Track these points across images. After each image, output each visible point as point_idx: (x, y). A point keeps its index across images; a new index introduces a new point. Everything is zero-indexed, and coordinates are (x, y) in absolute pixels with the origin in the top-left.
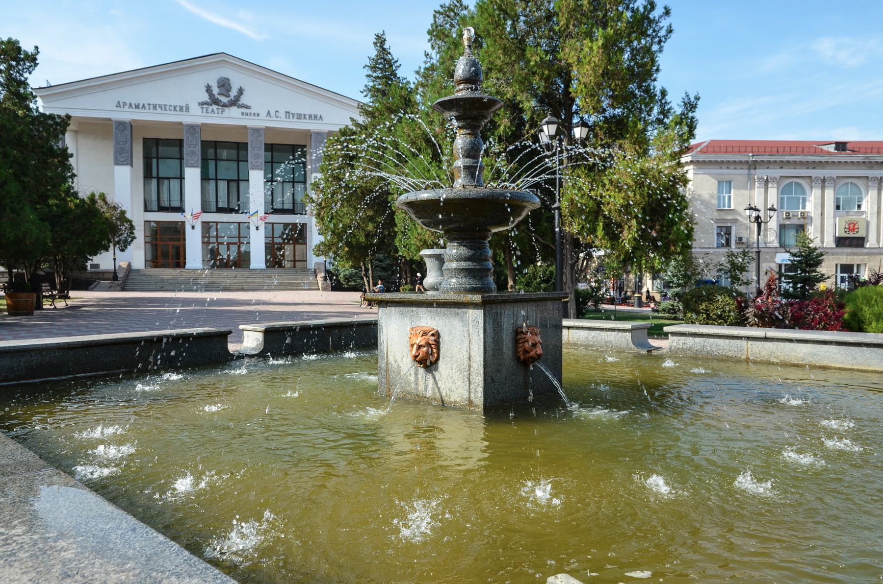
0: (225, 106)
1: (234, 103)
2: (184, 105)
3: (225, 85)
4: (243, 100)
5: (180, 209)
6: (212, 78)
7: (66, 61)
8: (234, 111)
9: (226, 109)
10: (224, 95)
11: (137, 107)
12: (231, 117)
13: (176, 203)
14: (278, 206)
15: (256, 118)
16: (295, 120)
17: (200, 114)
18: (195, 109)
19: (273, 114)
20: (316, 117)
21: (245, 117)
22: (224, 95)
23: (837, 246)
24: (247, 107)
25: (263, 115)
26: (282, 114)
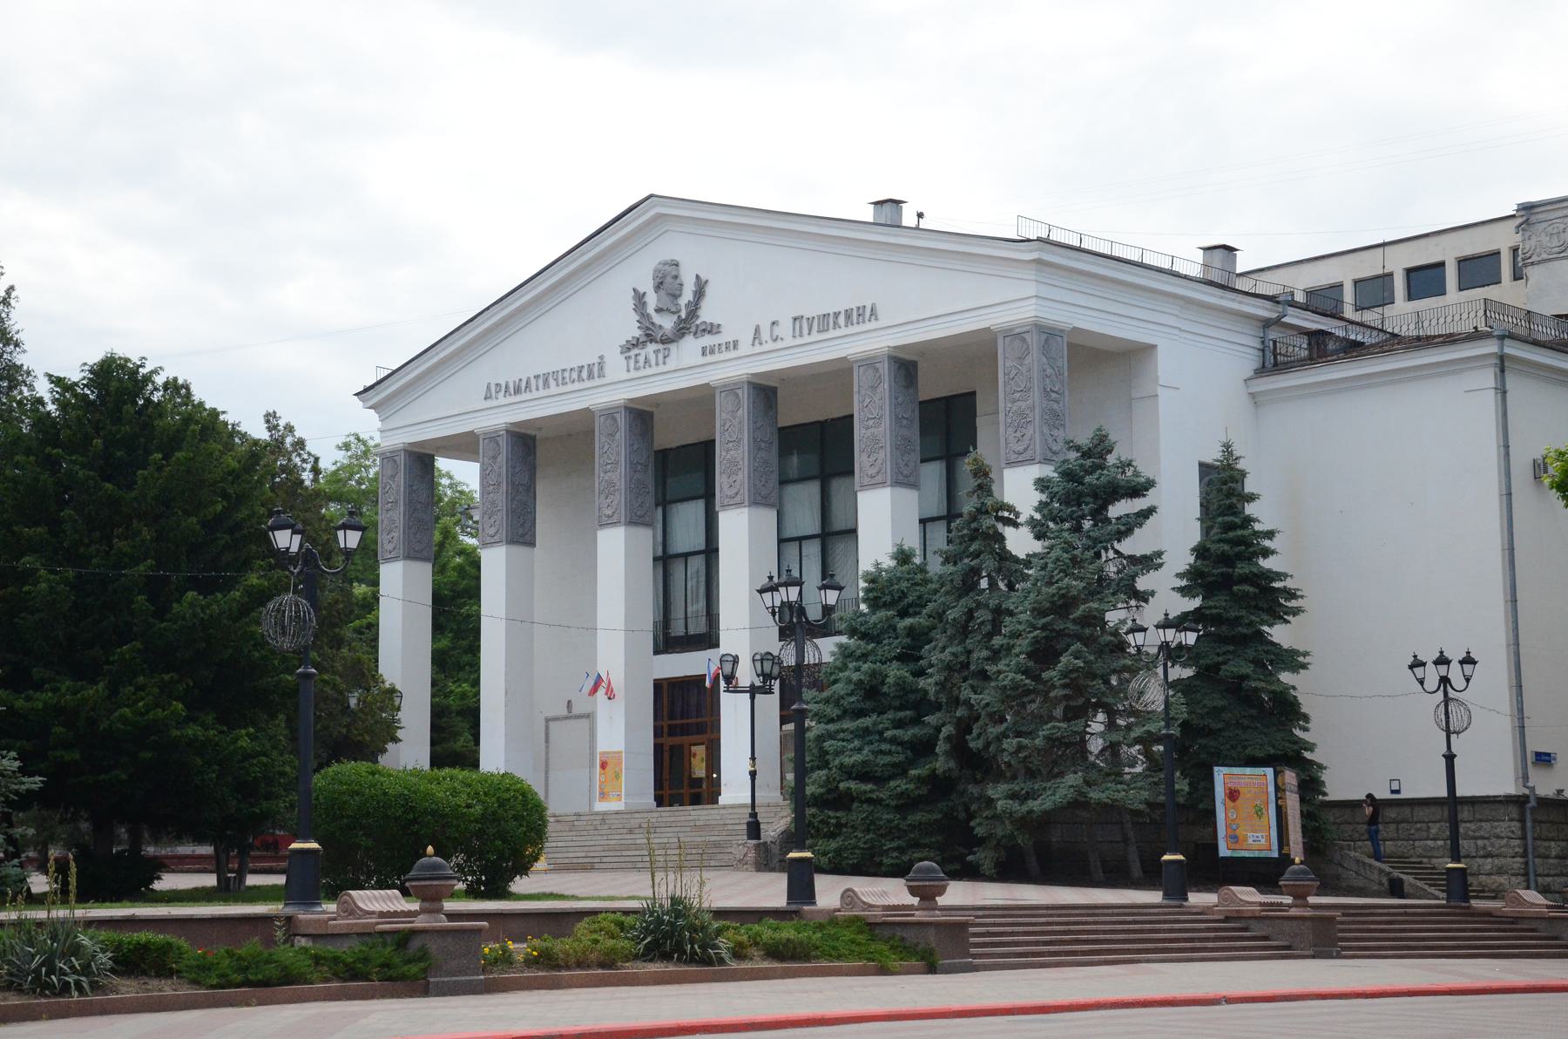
0: (666, 341)
1: (685, 327)
2: (596, 360)
3: (667, 280)
4: (706, 314)
5: (708, 639)
6: (638, 273)
7: (292, 356)
8: (690, 348)
9: (673, 347)
10: (674, 313)
11: (517, 391)
12: (683, 369)
13: (698, 627)
14: (678, 629)
15: (733, 354)
16: (554, 389)
17: (626, 376)
18: (617, 367)
19: (765, 335)
20: (861, 311)
21: (709, 358)
22: (674, 313)
23: (660, 801)
24: (712, 329)
25: (746, 338)
26: (785, 329)
